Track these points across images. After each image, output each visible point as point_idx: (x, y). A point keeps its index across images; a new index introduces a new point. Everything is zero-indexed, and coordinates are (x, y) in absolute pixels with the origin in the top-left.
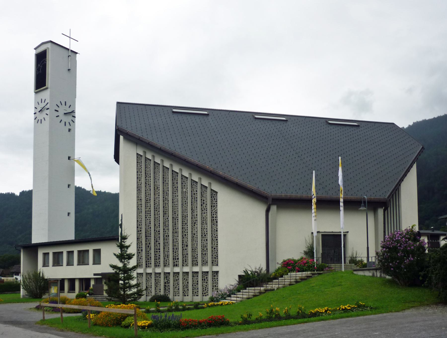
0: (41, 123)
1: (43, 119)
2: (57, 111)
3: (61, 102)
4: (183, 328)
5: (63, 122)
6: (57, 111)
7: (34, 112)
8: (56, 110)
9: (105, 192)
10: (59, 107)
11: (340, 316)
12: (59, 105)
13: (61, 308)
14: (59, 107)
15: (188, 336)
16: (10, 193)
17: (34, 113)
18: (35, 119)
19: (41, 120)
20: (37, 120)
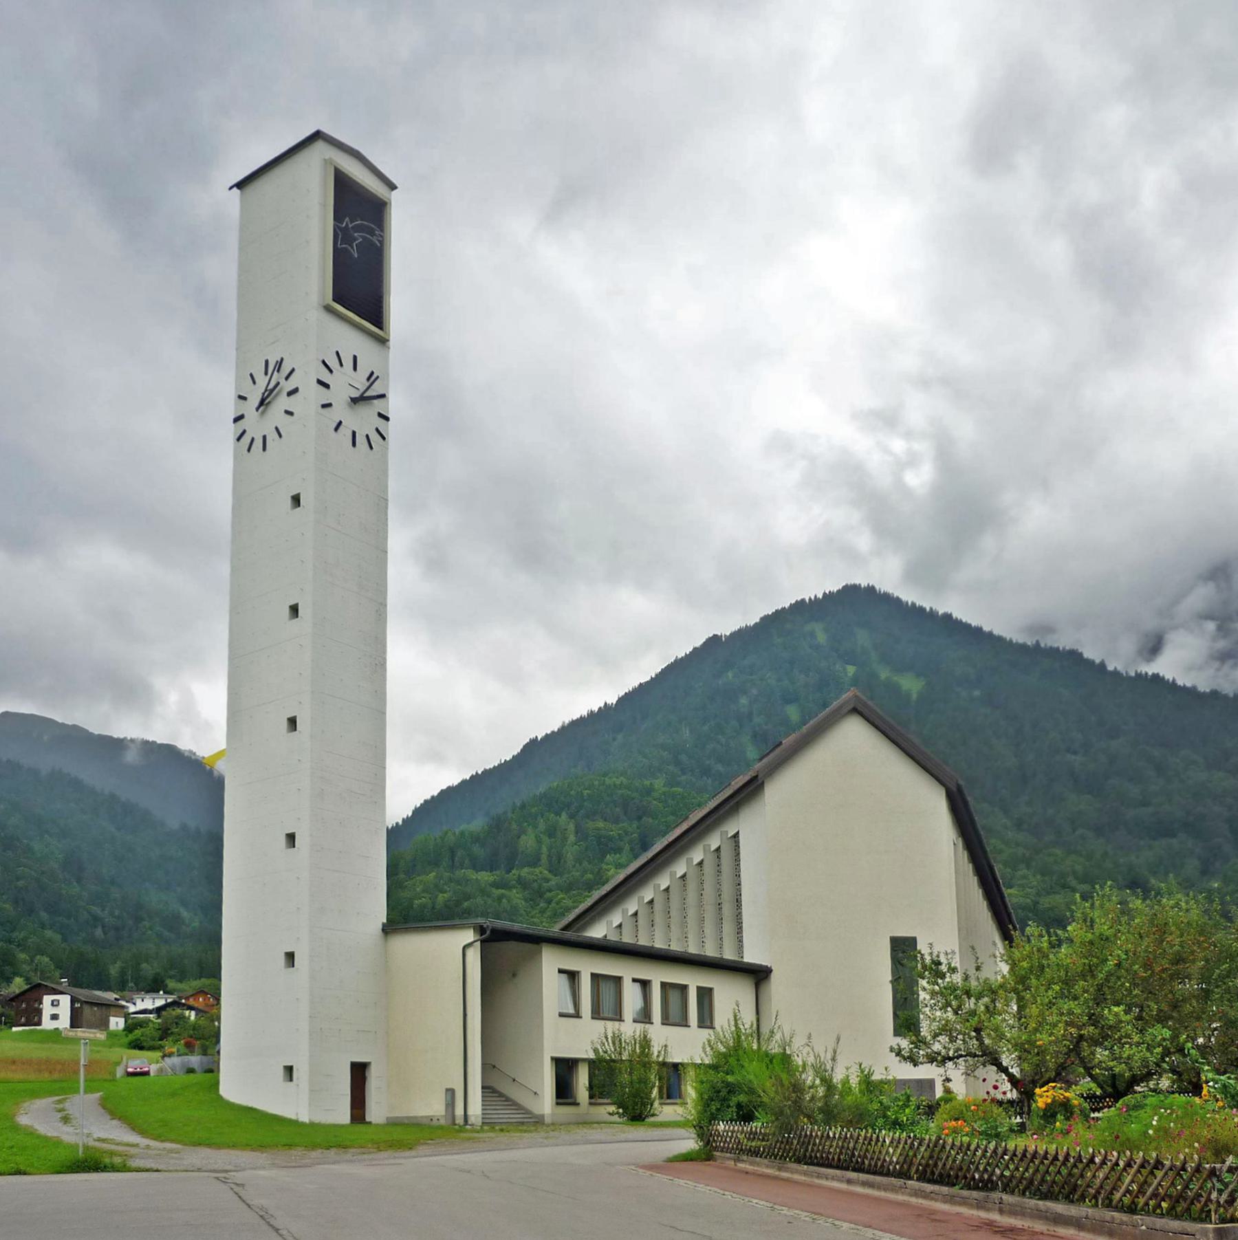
0: (264, 449)
1: (242, 440)
2: (327, 386)
3: (337, 353)
4: (912, 1051)
5: (345, 433)
6: (327, 386)
7: (236, 409)
8: (320, 382)
9: (797, 601)
10: (331, 371)
11: (553, 877)
12: (333, 362)
13: (881, 1191)
14: (331, 371)
15: (22, 1168)
16: (1061, 649)
17: (233, 417)
18: (239, 439)
19: (264, 438)
20: (246, 440)
